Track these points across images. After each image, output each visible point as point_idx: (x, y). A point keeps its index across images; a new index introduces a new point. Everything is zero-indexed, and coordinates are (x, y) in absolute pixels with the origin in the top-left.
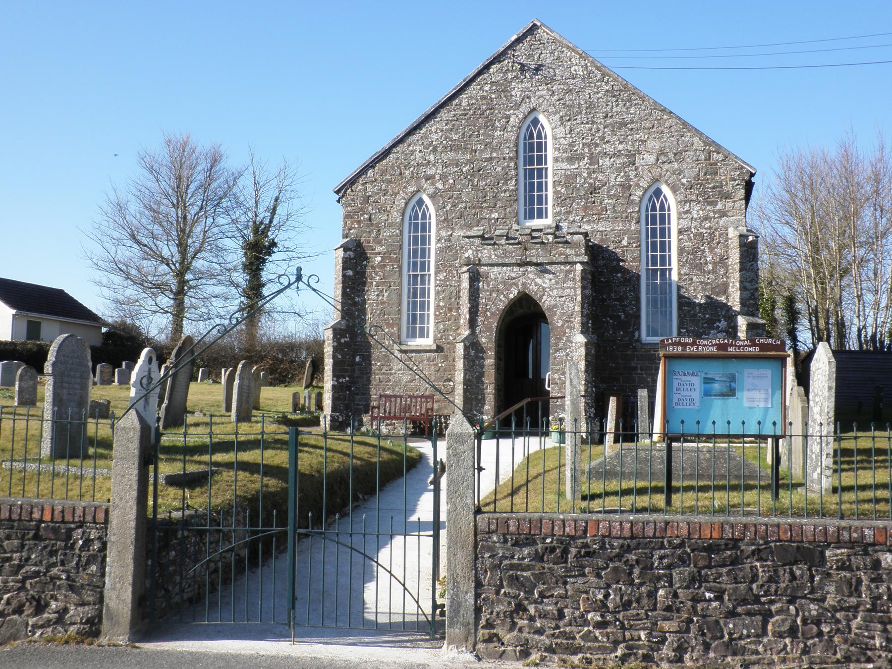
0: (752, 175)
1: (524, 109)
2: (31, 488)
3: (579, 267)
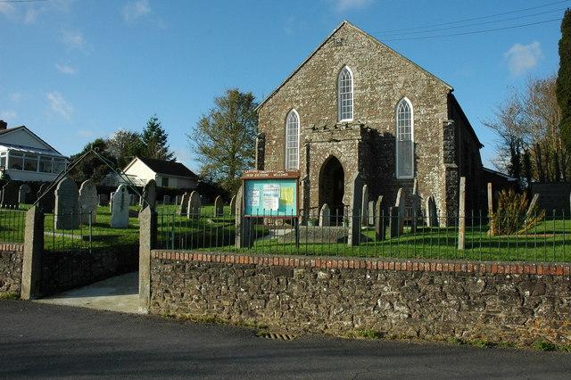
0: (453, 90)
1: (340, 65)
3: (357, 142)
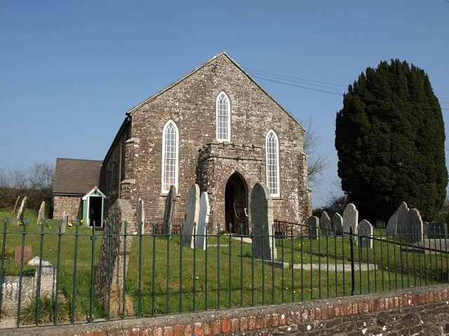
2: (393, 278)
